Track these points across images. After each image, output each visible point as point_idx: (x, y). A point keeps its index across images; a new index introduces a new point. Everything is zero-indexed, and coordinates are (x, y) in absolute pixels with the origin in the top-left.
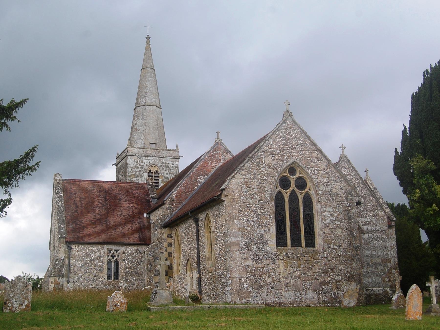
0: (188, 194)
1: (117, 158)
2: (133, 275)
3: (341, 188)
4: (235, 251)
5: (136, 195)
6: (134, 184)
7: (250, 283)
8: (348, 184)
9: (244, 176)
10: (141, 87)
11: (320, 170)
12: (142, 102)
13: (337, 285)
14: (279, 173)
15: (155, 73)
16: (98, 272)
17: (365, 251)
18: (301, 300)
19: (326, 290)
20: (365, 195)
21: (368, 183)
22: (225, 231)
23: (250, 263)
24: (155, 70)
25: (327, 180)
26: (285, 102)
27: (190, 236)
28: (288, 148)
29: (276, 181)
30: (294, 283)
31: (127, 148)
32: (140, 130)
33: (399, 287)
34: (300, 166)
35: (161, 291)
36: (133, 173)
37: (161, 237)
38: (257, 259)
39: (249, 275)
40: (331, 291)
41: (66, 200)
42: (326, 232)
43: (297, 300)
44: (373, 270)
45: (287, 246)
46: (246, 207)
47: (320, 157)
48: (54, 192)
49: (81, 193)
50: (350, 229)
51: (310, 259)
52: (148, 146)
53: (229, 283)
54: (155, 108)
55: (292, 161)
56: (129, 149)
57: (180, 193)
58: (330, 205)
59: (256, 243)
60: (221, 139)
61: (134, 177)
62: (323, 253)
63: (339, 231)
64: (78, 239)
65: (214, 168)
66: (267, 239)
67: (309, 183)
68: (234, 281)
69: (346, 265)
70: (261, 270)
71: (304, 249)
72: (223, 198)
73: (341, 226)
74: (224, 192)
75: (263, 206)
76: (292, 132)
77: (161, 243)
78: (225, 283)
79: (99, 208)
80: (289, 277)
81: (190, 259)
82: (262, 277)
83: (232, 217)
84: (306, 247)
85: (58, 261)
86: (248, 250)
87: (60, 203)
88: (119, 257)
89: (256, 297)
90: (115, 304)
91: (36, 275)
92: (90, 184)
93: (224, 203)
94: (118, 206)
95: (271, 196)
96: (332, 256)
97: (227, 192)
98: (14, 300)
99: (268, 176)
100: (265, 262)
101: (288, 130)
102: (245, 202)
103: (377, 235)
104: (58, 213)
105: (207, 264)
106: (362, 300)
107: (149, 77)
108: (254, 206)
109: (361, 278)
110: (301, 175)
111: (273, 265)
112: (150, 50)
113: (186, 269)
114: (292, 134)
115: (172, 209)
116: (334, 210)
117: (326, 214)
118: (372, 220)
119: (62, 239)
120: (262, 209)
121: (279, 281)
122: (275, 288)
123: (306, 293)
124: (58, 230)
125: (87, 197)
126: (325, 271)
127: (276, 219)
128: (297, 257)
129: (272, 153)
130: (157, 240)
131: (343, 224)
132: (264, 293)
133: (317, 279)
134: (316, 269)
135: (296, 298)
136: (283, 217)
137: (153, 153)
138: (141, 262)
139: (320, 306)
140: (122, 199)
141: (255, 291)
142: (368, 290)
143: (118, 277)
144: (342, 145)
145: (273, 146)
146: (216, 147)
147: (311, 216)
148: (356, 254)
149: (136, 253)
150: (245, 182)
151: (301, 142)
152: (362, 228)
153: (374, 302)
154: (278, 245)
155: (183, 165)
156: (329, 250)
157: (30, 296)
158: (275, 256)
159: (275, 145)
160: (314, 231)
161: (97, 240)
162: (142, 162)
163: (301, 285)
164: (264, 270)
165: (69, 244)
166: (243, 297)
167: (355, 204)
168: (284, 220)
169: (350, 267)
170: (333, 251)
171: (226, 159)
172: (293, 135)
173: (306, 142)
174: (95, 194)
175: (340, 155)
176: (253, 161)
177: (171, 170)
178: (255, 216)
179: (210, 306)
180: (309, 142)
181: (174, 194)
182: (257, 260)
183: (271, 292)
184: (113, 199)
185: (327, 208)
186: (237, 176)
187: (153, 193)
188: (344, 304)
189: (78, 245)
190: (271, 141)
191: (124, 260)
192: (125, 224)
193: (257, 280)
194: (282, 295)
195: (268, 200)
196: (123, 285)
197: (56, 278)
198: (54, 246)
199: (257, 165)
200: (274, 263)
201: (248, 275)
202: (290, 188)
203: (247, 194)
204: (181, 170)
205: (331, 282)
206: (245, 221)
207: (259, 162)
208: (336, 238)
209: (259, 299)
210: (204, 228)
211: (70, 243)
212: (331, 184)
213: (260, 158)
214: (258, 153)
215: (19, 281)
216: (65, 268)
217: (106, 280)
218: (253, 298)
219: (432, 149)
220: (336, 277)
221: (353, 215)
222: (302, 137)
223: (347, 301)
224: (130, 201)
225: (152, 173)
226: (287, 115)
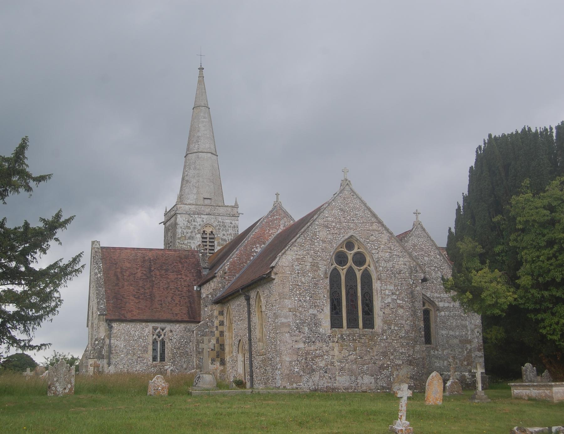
0: (242, 265)
1: (165, 215)
2: (181, 356)
3: (405, 264)
6: (183, 251)
7: (301, 367)
8: (413, 259)
10: (193, 130)
12: (194, 148)
14: (335, 248)
15: (210, 113)
16: (143, 353)
18: (356, 385)
22: (275, 312)
23: (301, 345)
24: (209, 108)
26: (342, 170)
27: (242, 314)
28: (346, 221)
29: (331, 258)
31: (176, 204)
32: (192, 182)
35: (204, 375)
36: (184, 234)
37: (212, 314)
38: (309, 341)
41: (106, 272)
42: (386, 312)
44: (450, 352)
45: (342, 328)
47: (381, 230)
48: (92, 262)
50: (413, 309)
51: (367, 342)
52: (201, 202)
53: (278, 367)
54: (209, 155)
55: (349, 235)
56: (178, 206)
57: (233, 264)
60: (280, 202)
61: (185, 240)
62: (383, 334)
63: (401, 311)
64: (119, 316)
65: (272, 235)
67: (368, 259)
68: (284, 365)
70: (314, 353)
71: (361, 331)
73: (404, 305)
74: (274, 270)
77: (212, 321)
78: (275, 367)
79: (142, 281)
81: (242, 340)
82: (315, 360)
83: (282, 296)
84: (363, 328)
85: (98, 341)
86: (300, 332)
87: (99, 275)
88: (166, 336)
90: (156, 388)
91: (70, 354)
93: (275, 282)
94: (165, 278)
96: (393, 338)
97: (277, 269)
98: (57, 384)
99: (322, 252)
100: (318, 345)
103: (456, 312)
104: (96, 287)
105: (258, 346)
107: (203, 117)
108: (306, 284)
109: (424, 362)
110: (359, 250)
111: (326, 348)
112: (203, 84)
113: (238, 350)
114: (350, 205)
115: (224, 283)
116: (396, 288)
117: (387, 292)
119: (102, 317)
120: (316, 288)
123: (362, 378)
124: (97, 306)
125: (129, 268)
126: (385, 354)
127: (330, 298)
128: (354, 339)
130: (207, 318)
132: (316, 377)
133: (375, 363)
134: (374, 352)
135: (351, 383)
136: (339, 296)
137: (208, 210)
138: (191, 341)
139: (378, 392)
140: (169, 270)
142: (443, 375)
143: (164, 358)
144: (417, 210)
146: (275, 211)
149: (184, 331)
151: (360, 213)
152: (438, 305)
154: (333, 325)
155: (243, 226)
157: (73, 380)
159: (331, 217)
160: (373, 311)
161: (141, 317)
164: (317, 353)
165: (109, 321)
166: (293, 382)
167: (420, 281)
171: (286, 225)
174: (139, 264)
176: (306, 236)
177: (229, 231)
179: (253, 391)
180: (369, 213)
181: (227, 266)
182: (309, 342)
184: (158, 270)
186: (288, 252)
187: (205, 262)
189: (120, 323)
190: (326, 214)
191: (171, 339)
192: (172, 298)
196: (169, 368)
197: (95, 359)
198: (92, 324)
199: (310, 240)
200: (328, 346)
201: (299, 358)
202: (347, 264)
204: (240, 232)
207: (312, 237)
208: (397, 318)
209: (310, 384)
210: (255, 307)
211: (111, 321)
215: (62, 366)
216: (106, 348)
217: (151, 362)
221: (417, 293)
222: (361, 208)
223: (397, 386)
224: (179, 272)
225: (206, 234)
226: (346, 183)
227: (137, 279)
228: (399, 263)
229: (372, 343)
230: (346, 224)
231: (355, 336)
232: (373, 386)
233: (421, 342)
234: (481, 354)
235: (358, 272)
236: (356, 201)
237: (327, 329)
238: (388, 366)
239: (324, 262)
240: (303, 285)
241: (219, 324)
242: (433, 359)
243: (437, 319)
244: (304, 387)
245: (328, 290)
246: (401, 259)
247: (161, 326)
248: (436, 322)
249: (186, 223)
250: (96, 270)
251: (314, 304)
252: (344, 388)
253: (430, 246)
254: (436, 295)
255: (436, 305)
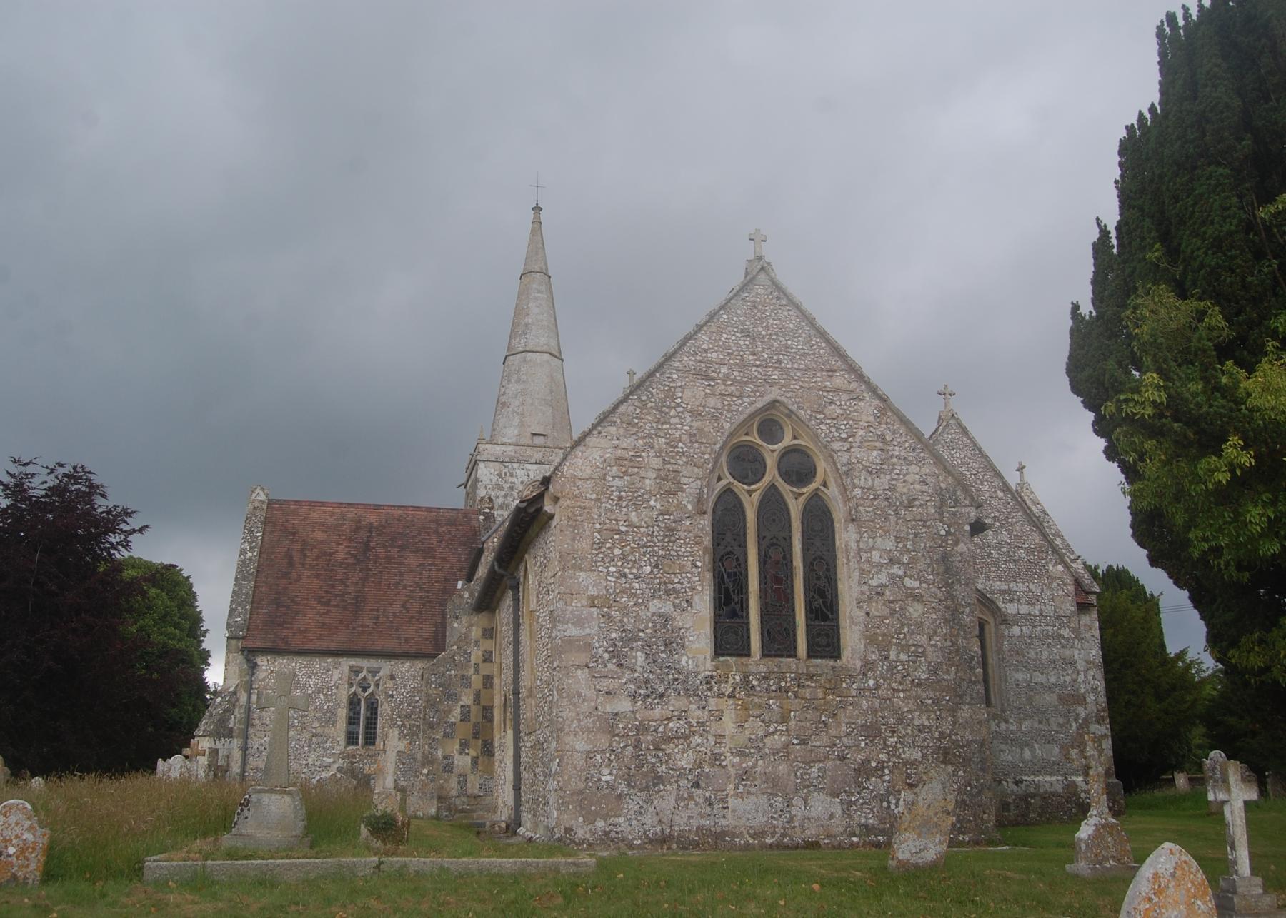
3: (924, 481)
4: (576, 669)
5: (446, 538)
8: (945, 469)
9: (613, 442)
11: (856, 426)
13: (909, 776)
14: (726, 434)
16: (324, 726)
17: (1013, 672)
18: (788, 822)
19: (872, 791)
20: (1010, 520)
21: (1026, 498)
23: (624, 705)
25: (879, 455)
28: (758, 363)
30: (767, 771)
32: (512, 406)
33: (1100, 791)
34: (793, 412)
35: (265, 798)
38: (647, 693)
39: (619, 743)
40: (889, 794)
42: (874, 613)
43: (775, 822)
44: (1036, 725)
45: (748, 655)
46: (616, 534)
49: (310, 533)
50: (949, 603)
51: (820, 695)
54: (547, 357)
55: (768, 398)
58: (888, 531)
59: (644, 643)
62: (865, 674)
63: (915, 610)
66: (682, 631)
67: (822, 466)
69: (938, 713)
70: (661, 729)
72: (548, 507)
73: (923, 593)
75: (673, 530)
76: (770, 316)
77: (465, 652)
79: (345, 568)
80: (752, 750)
82: (663, 750)
83: (570, 562)
84: (809, 657)
86: (620, 665)
87: (250, 554)
89: (641, 813)
92: (337, 511)
93: (554, 523)
94: (395, 563)
95: (699, 501)
97: (558, 487)
99: (691, 441)
101: (759, 311)
102: (613, 517)
103: (1047, 628)
106: (989, 822)
108: (642, 530)
110: (796, 442)
111: (699, 712)
114: (771, 321)
116: (901, 545)
117: (876, 556)
118: (1031, 586)
119: (233, 642)
120: (670, 541)
121: (717, 763)
122: (704, 785)
123: (805, 801)
125: (322, 542)
126: (871, 732)
128: (780, 688)
129: (705, 376)
131: (929, 589)
132: (666, 800)
133: (843, 758)
134: (839, 725)
135: (772, 818)
136: (740, 565)
137: (538, 455)
141: (639, 794)
142: (1022, 782)
144: (946, 387)
145: (709, 355)
147: (827, 564)
148: (970, 680)
150: (617, 459)
152: (1004, 610)
153: (1040, 815)
154: (721, 648)
156: (882, 667)
158: (707, 684)
160: (838, 610)
161: (323, 645)
162: (511, 475)
163: (789, 775)
164: (671, 730)
166: (596, 814)
167: (967, 528)
168: (741, 573)
169: (950, 719)
170: (895, 671)
172: (772, 324)
173: (814, 345)
174: (344, 535)
175: (940, 412)
176: (644, 398)
178: (645, 561)
179: (381, 863)
180: (824, 345)
182: (648, 696)
183: (691, 797)
184: (385, 547)
185: (879, 540)
188: (901, 856)
191: (392, 696)
192: (403, 606)
193: (646, 759)
194: (728, 807)
195: (690, 512)
196: (334, 762)
199: (657, 410)
200: (704, 708)
201: (614, 744)
202: (764, 480)
203: (623, 493)
205: (887, 767)
206: (612, 576)
208: (906, 630)
209: (649, 819)
212: (891, 467)
213: (666, 388)
214: (661, 375)
216: (239, 713)
217: (342, 747)
218: (629, 817)
219: (1213, 263)
220: (906, 749)
221: (960, 561)
226: (758, 269)
227: (333, 565)
228: (909, 478)
229: (834, 699)
230: (760, 370)
231: (784, 679)
232: (837, 825)
233: (975, 695)
234: (1103, 729)
235: (794, 501)
236: (786, 313)
237: (701, 657)
238: (881, 766)
239: (696, 470)
240: (633, 531)
241: (481, 658)
242: (995, 742)
243: (1002, 644)
244: (629, 828)
245: (706, 548)
246: (914, 468)
247: (369, 666)
248: (1000, 651)
249: (494, 479)
250: (246, 544)
251: (663, 587)
252: (751, 832)
253: (980, 470)
254: (999, 585)
255: (999, 609)
